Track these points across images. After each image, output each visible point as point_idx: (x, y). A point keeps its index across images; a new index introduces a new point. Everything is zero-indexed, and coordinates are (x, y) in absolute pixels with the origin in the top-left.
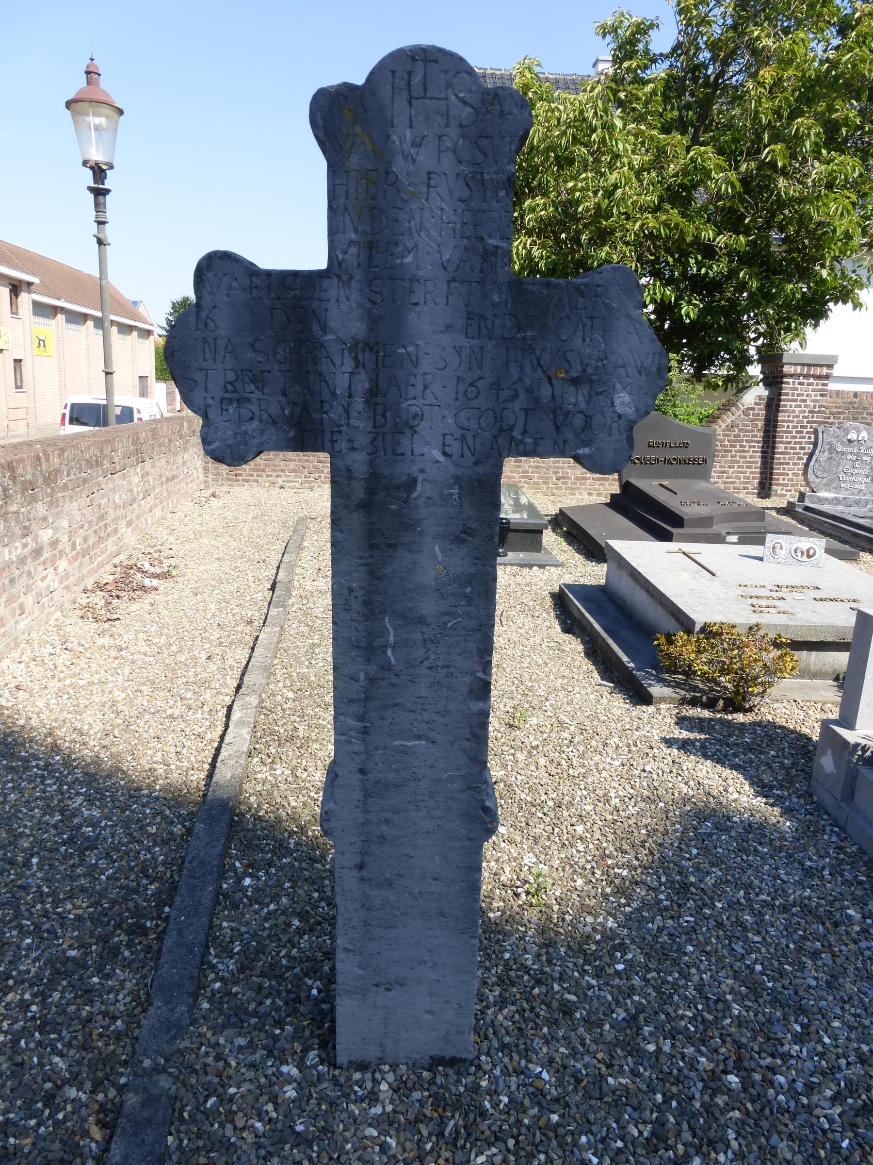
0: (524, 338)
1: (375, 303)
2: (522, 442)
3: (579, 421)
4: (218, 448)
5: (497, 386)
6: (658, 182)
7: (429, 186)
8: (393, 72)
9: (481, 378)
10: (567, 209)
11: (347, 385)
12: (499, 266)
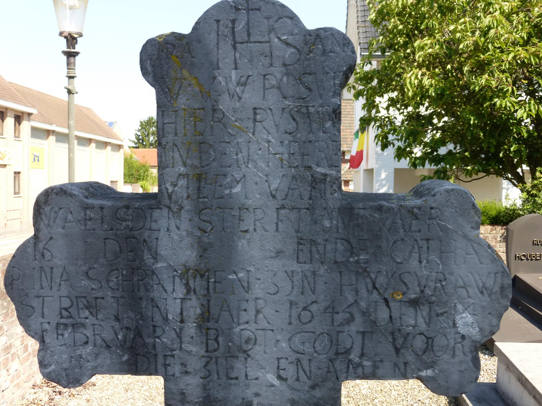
0: (357, 262)
1: (205, 232)
2: (360, 365)
3: (419, 343)
4: (54, 371)
5: (331, 309)
6: (526, 21)
7: (255, 120)
8: (218, 21)
9: (315, 302)
10: (451, 48)
11: (179, 311)
12: (328, 192)
